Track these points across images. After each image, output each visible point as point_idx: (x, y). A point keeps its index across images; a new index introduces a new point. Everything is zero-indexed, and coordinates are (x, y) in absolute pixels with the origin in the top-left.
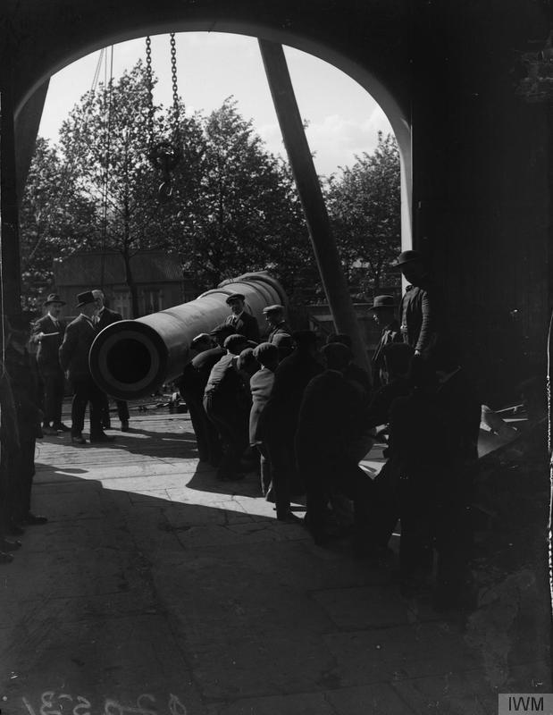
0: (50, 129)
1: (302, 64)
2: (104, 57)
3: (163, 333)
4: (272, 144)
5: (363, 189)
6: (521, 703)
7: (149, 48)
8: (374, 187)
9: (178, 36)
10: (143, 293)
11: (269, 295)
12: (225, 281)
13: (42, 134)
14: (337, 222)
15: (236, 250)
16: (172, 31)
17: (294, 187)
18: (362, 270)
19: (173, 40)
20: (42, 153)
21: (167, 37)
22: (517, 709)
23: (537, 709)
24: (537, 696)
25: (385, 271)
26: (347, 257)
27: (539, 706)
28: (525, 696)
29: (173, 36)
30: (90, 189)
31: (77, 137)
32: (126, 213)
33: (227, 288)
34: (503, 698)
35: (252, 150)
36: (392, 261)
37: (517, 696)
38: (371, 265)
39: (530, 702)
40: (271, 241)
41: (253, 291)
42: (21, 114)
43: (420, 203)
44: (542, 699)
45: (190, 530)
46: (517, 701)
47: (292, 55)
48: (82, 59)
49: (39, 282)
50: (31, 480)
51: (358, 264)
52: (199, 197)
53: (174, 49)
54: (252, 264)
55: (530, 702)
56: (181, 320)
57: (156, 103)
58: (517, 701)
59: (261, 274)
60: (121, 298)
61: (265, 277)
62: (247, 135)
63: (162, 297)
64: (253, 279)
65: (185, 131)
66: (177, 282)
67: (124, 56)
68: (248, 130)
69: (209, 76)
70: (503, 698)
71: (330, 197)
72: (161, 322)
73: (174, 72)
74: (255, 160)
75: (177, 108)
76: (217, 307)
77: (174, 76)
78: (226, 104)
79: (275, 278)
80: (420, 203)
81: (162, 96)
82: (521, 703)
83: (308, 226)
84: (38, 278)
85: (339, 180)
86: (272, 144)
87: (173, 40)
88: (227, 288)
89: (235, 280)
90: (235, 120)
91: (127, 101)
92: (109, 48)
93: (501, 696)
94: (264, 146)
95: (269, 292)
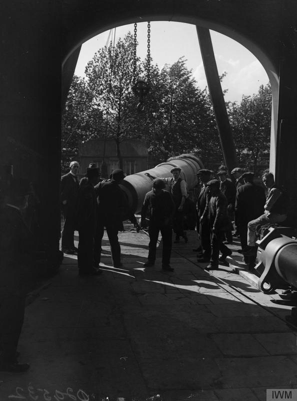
0: (80, 72)
1: (218, 39)
2: (111, 35)
3: (135, 186)
4: (201, 82)
5: (251, 110)
6: (279, 395)
7: (136, 29)
8: (256, 111)
9: (151, 23)
10: (125, 162)
11: (195, 167)
12: (171, 158)
14: (236, 129)
15: (178, 141)
17: (212, 108)
18: (248, 155)
19: (149, 25)
21: (147, 23)
22: (277, 398)
23: (288, 398)
24: (288, 391)
25: (260, 156)
26: (239, 148)
27: (289, 396)
29: (149, 23)
30: (99, 103)
31: (95, 77)
32: (118, 119)
33: (171, 162)
34: (269, 392)
35: (190, 84)
36: (264, 150)
38: (253, 152)
39: (284, 393)
40: (197, 137)
41: (186, 164)
42: (64, 65)
44: (291, 392)
45: (145, 295)
46: (277, 393)
47: (215, 35)
49: (71, 154)
51: (245, 151)
52: (162, 110)
53: (149, 30)
54: (186, 149)
55: (284, 393)
56: (221, 78)
57: (138, 55)
58: (277, 393)
59: (191, 155)
60: (114, 164)
61: (193, 156)
62: (188, 78)
63: (136, 165)
64: (185, 157)
65: (152, 74)
66: (144, 157)
67: (121, 32)
68: (189, 75)
69: (167, 45)
70: (269, 392)
71: (232, 114)
72: (135, 179)
73: (149, 43)
74: (190, 90)
75: (148, 65)
76: (166, 172)
77: (149, 45)
78: (180, 61)
79: (198, 157)
81: (141, 53)
82: (279, 395)
83: (218, 130)
85: (239, 104)
86: (201, 82)
87: (149, 25)
88: (171, 162)
89: (177, 157)
91: (120, 58)
92: (114, 29)
93: (268, 390)
94: (196, 84)
95: (195, 166)
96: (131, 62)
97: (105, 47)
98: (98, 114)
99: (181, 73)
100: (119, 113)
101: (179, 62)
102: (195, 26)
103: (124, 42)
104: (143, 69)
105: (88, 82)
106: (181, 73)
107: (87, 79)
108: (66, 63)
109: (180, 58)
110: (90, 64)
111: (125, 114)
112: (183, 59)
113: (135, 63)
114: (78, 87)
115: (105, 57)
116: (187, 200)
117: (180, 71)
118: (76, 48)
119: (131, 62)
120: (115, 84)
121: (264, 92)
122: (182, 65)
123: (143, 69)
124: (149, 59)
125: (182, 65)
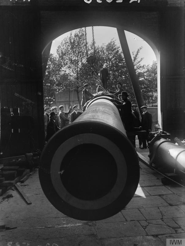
6: (174, 242)
13: (51, 52)
16: (92, 26)
20: (51, 59)
21: (91, 27)
22: (173, 244)
23: (180, 244)
28: (175, 239)
31: (62, 55)
32: (77, 78)
37: (173, 240)
39: (177, 241)
43: (12, 130)
47: (127, 33)
48: (62, 35)
50: (121, 210)
55: (177, 241)
78: (112, 41)
80: (12, 130)
81: (90, 41)
82: (174, 242)
84: (50, 99)
90: (114, 46)
93: (167, 239)
96: (83, 45)
97: (68, 37)
98: (65, 77)
99: (114, 48)
100: (77, 75)
101: (111, 42)
102: (116, 28)
103: (78, 33)
104: (90, 49)
105: (59, 58)
106: (114, 48)
107: (58, 56)
108: (45, 50)
109: (112, 40)
110: (59, 47)
111: (81, 76)
112: (113, 40)
113: (86, 45)
114: (53, 61)
115: (67, 43)
116: (4, 166)
117: (113, 47)
118: (51, 42)
119: (83, 45)
120: (74, 58)
121: (155, 64)
122: (114, 44)
123: (90, 49)
124: (94, 43)
125: (114, 44)
